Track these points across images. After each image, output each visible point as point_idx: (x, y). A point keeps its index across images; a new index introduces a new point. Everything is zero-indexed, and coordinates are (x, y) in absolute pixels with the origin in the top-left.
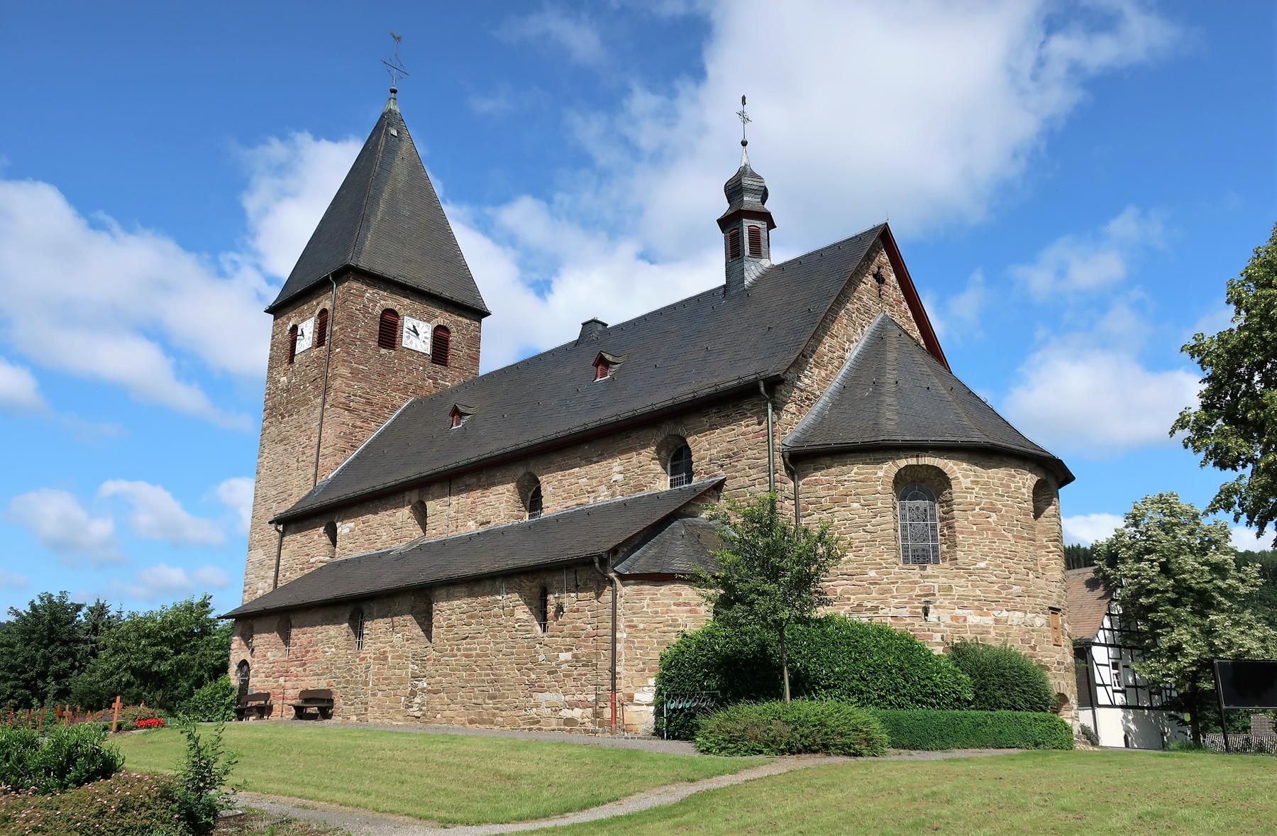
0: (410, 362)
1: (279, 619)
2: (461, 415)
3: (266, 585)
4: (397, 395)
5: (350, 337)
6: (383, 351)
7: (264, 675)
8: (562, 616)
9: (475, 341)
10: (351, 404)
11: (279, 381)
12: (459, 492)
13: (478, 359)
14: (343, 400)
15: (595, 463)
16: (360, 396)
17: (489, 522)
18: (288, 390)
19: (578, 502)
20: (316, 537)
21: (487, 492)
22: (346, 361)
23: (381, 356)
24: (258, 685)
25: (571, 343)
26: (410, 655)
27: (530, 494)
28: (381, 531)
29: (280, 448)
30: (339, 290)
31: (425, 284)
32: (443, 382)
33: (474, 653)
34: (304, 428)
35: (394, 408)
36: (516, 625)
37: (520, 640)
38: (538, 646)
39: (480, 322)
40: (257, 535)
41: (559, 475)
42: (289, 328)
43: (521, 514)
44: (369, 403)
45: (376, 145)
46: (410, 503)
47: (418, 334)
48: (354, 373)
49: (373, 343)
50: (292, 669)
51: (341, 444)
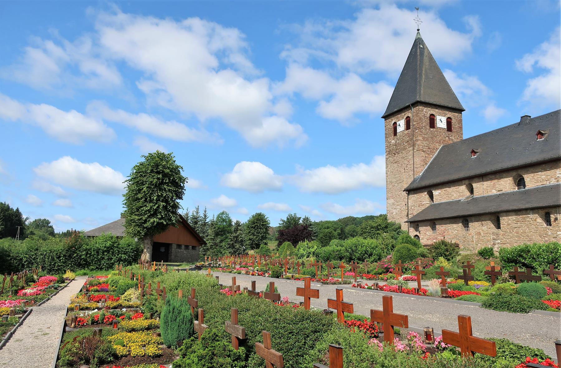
0: (440, 132)
1: (430, 222)
2: (475, 153)
4: (437, 144)
5: (421, 126)
6: (432, 129)
8: (557, 221)
9: (460, 121)
10: (424, 149)
11: (391, 142)
12: (487, 180)
13: (462, 128)
14: (421, 148)
15: (548, 171)
16: (426, 146)
17: (502, 190)
18: (396, 145)
19: (542, 184)
20: (424, 196)
21: (500, 181)
22: (421, 135)
23: (431, 131)
24: (424, 242)
25: (515, 124)
26: (491, 233)
27: (517, 181)
28: (453, 193)
29: (395, 165)
30: (414, 110)
31: (443, 103)
32: (451, 138)
33: (520, 232)
34: (405, 158)
36: (538, 224)
37: (539, 228)
38: (548, 230)
39: (461, 114)
41: (532, 175)
42: (392, 123)
43: (515, 187)
44: (429, 148)
45: (416, 52)
46: (465, 184)
47: (442, 122)
48: (424, 138)
49: (428, 127)
50: (439, 237)
51: (422, 163)
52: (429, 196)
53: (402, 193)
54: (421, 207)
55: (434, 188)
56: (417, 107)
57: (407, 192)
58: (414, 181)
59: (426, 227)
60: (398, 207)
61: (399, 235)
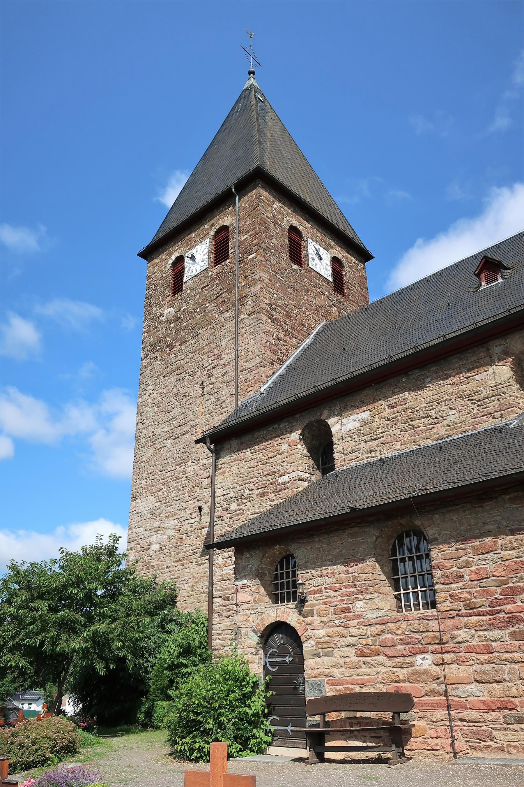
3: (164, 537)
7: (351, 651)
20: (285, 447)
24: (337, 673)
29: (171, 380)
35: (310, 329)
40: (144, 481)
42: (170, 262)
46: (506, 354)
47: (321, 259)
52: (310, 450)
53: (188, 469)
54: (271, 496)
55: (338, 407)
56: (254, 191)
57: (212, 447)
58: (238, 410)
59: (346, 563)
60: (172, 522)
61: (165, 636)
